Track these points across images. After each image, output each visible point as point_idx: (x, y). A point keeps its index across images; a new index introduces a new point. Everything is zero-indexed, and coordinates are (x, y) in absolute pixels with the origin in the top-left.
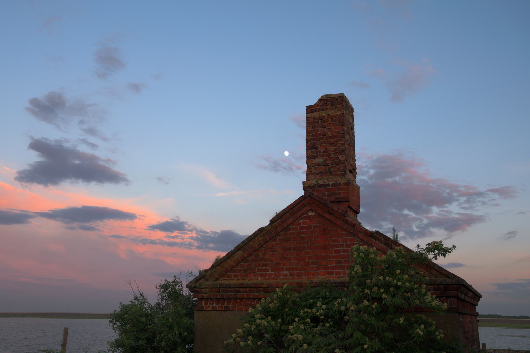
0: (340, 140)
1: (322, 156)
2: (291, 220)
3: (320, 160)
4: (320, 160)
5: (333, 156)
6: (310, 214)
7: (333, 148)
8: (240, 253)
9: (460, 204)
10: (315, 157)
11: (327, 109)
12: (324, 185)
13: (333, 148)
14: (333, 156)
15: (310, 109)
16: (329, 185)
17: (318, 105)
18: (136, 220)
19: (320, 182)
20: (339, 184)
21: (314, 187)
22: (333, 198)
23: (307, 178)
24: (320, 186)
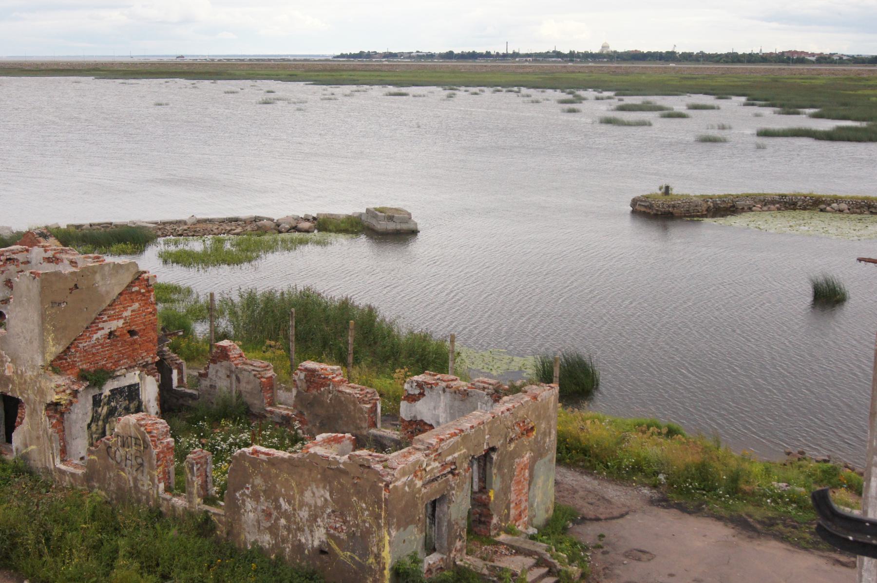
18: (755, 132)
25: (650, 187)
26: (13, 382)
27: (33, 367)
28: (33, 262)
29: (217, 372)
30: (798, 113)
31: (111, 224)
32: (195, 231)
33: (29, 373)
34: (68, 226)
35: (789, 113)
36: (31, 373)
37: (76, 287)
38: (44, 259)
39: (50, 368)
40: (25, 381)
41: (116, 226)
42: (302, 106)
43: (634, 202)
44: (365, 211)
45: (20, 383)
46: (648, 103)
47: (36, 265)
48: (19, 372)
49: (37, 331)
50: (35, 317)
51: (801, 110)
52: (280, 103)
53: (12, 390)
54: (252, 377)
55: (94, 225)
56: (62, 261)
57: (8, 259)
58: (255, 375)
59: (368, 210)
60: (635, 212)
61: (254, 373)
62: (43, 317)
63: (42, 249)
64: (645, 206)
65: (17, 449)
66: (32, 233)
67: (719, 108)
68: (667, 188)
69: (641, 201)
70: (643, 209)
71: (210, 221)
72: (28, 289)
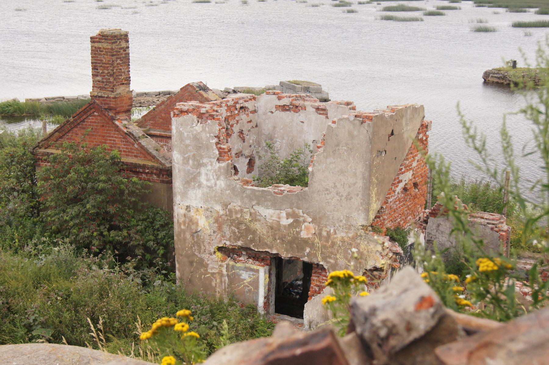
0: (110, 67)
1: (101, 76)
2: (85, 117)
3: (99, 78)
4: (99, 78)
5: (106, 77)
6: (95, 114)
7: (106, 72)
8: (57, 134)
9: (249, 274)
10: (97, 76)
11: (102, 42)
12: (101, 97)
13: (106, 72)
14: (106, 77)
15: (188, 85)
16: (104, 97)
17: (97, 38)
18: (511, 23)
19: (100, 94)
20: (110, 98)
21: (96, 97)
22: (106, 107)
23: (93, 90)
24: (99, 97)
25: (496, 62)
26: (312, 246)
27: (349, 227)
28: (260, 112)
29: (439, 225)
30: (525, 12)
31: (64, 98)
32: (140, 103)
33: (340, 235)
34: (27, 100)
35: (517, 12)
36: (343, 235)
37: (392, 134)
38: (278, 107)
39: (370, 228)
40: (333, 244)
41: (68, 100)
42: (136, 10)
43: (486, 75)
44: (278, 84)
45: (324, 247)
46: (402, 5)
47: (265, 114)
48: (324, 233)
49: (360, 184)
50: (360, 169)
51: (527, 9)
52: (113, 8)
53: (309, 255)
54: (488, 231)
55: (49, 99)
56: (304, 108)
57: (242, 108)
58: (492, 229)
59: (281, 83)
60: (486, 83)
61: (490, 226)
62: (370, 167)
63: (275, 97)
64: (499, 78)
65: (310, 323)
66: (192, 86)
67: (460, 9)
68: (515, 63)
69: (494, 73)
70: (496, 80)
71: (146, 94)
72: (351, 136)
